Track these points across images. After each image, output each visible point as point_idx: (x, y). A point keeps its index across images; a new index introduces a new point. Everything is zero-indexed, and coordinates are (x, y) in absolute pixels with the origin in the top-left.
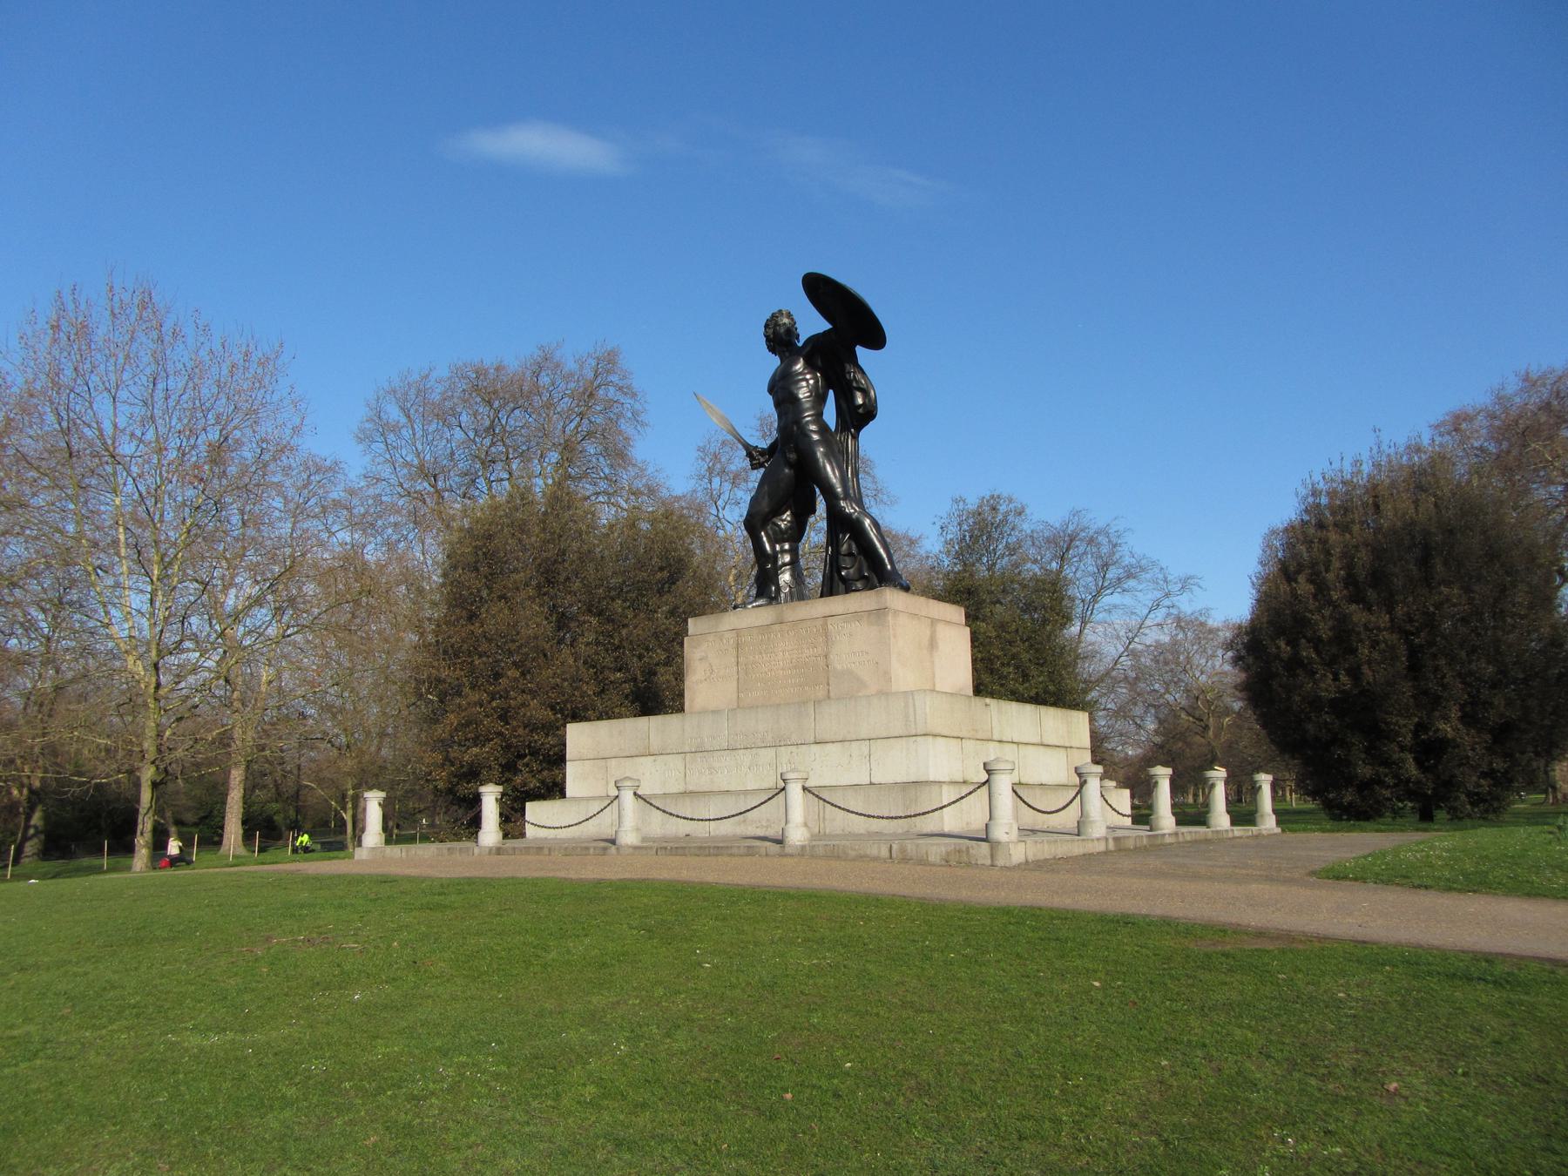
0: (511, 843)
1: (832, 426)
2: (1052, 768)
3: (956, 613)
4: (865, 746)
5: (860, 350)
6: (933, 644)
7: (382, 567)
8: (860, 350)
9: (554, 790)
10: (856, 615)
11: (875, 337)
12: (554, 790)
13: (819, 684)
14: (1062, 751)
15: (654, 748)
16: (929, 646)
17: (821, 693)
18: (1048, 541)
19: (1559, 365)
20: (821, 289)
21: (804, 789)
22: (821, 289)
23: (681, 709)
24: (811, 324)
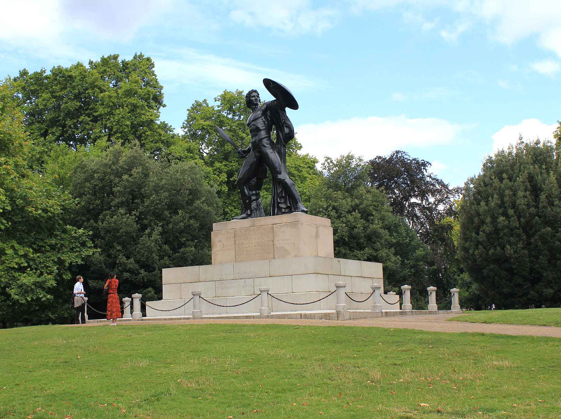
0: (144, 318)
1: (275, 141)
2: (365, 287)
3: (327, 222)
4: (290, 277)
5: (287, 109)
6: (317, 236)
7: (500, 223)
8: (287, 109)
9: (158, 296)
10: (286, 224)
11: (294, 105)
12: (158, 296)
13: (270, 251)
14: (370, 280)
15: (202, 279)
16: (311, 234)
17: (272, 256)
18: (160, 93)
19: (543, 134)
20: (269, 84)
21: (268, 294)
22: (269, 84)
23: (210, 263)
24: (266, 97)
